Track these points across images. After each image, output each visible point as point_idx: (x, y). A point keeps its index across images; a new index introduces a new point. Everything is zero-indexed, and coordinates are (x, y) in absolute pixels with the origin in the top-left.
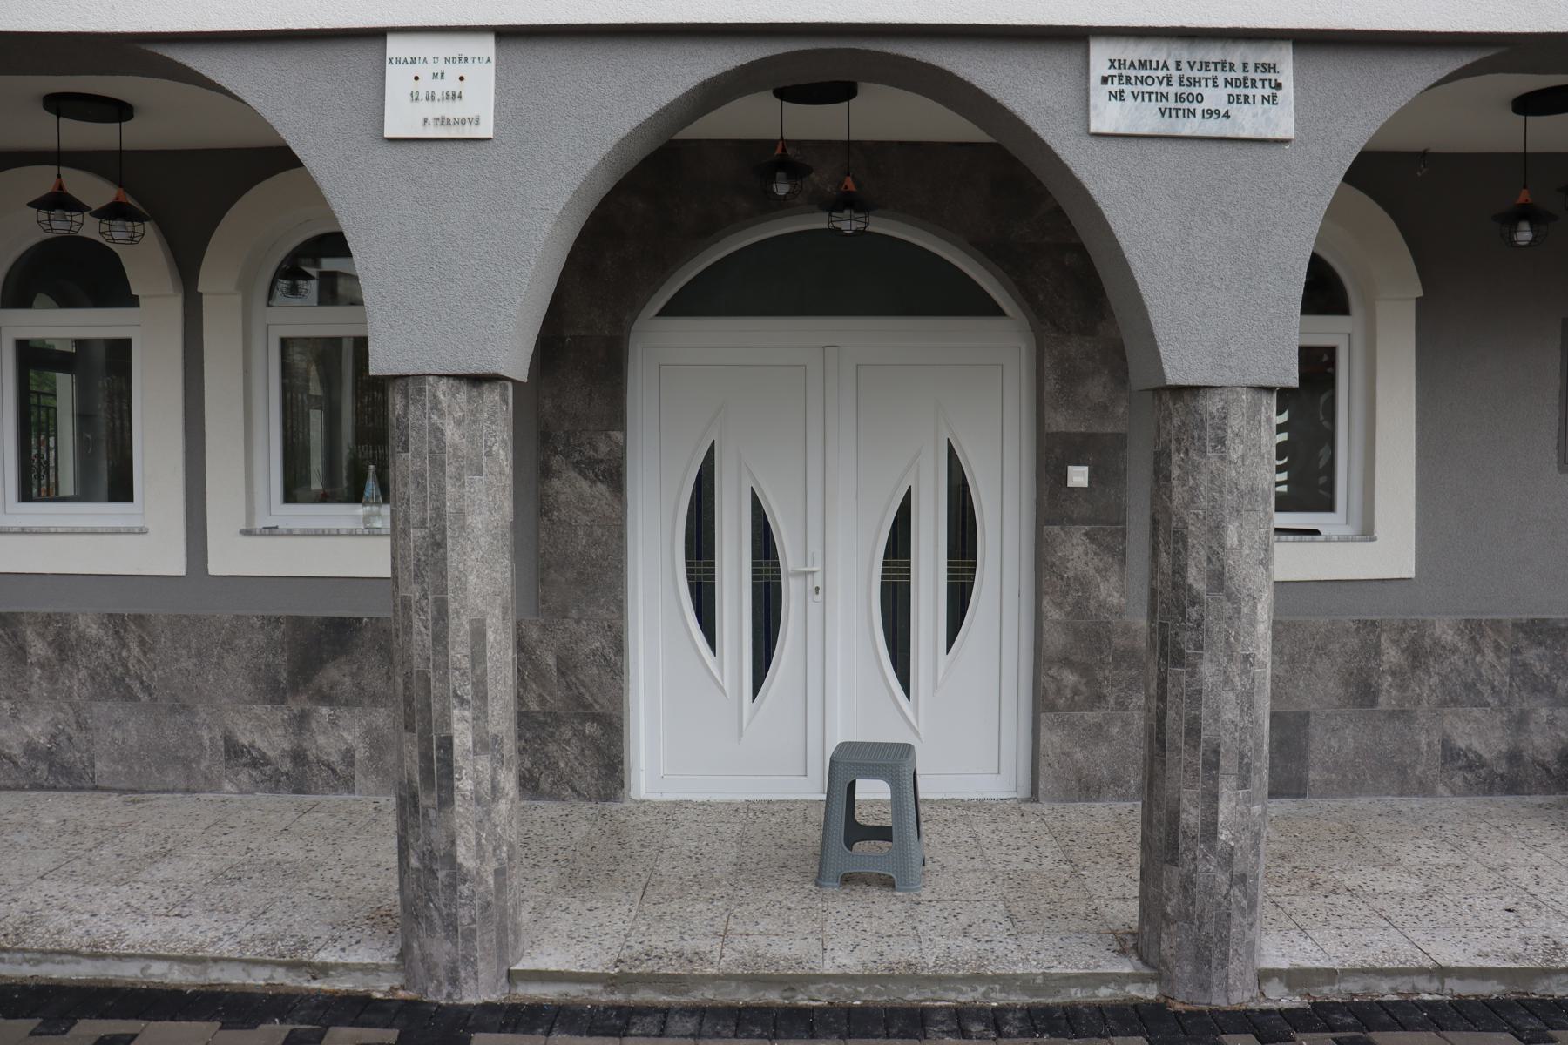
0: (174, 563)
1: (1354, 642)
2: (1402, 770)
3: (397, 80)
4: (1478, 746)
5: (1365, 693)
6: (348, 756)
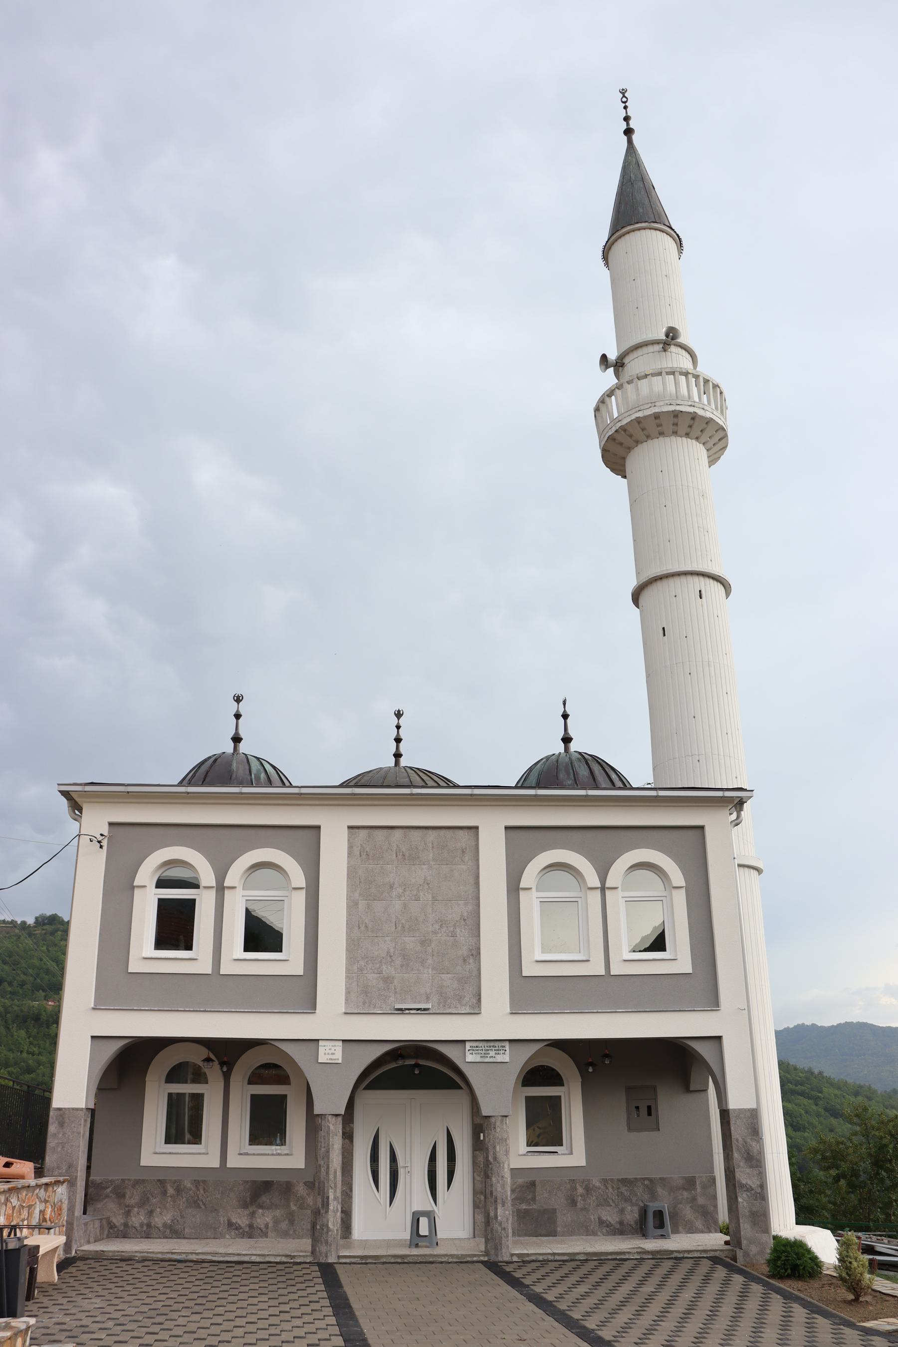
0: (216, 1164)
1: (568, 1186)
2: (586, 1227)
3: (321, 1050)
4: (609, 1219)
5: (573, 1202)
6: (267, 1226)
